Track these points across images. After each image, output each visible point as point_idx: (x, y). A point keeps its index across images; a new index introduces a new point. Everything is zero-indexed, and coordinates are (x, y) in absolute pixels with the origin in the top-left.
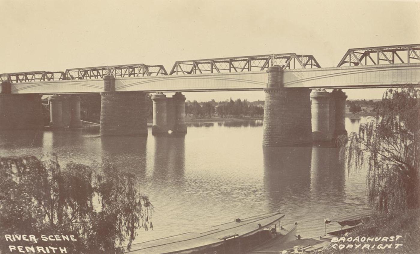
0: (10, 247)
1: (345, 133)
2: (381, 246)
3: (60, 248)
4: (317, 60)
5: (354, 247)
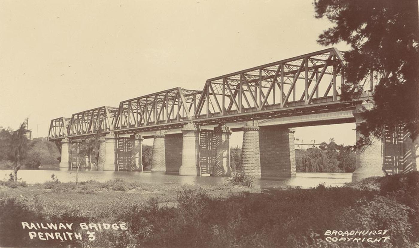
0: (23, 223)
1: (361, 134)
2: (371, 240)
3: (75, 233)
4: (302, 95)
5: (347, 239)
